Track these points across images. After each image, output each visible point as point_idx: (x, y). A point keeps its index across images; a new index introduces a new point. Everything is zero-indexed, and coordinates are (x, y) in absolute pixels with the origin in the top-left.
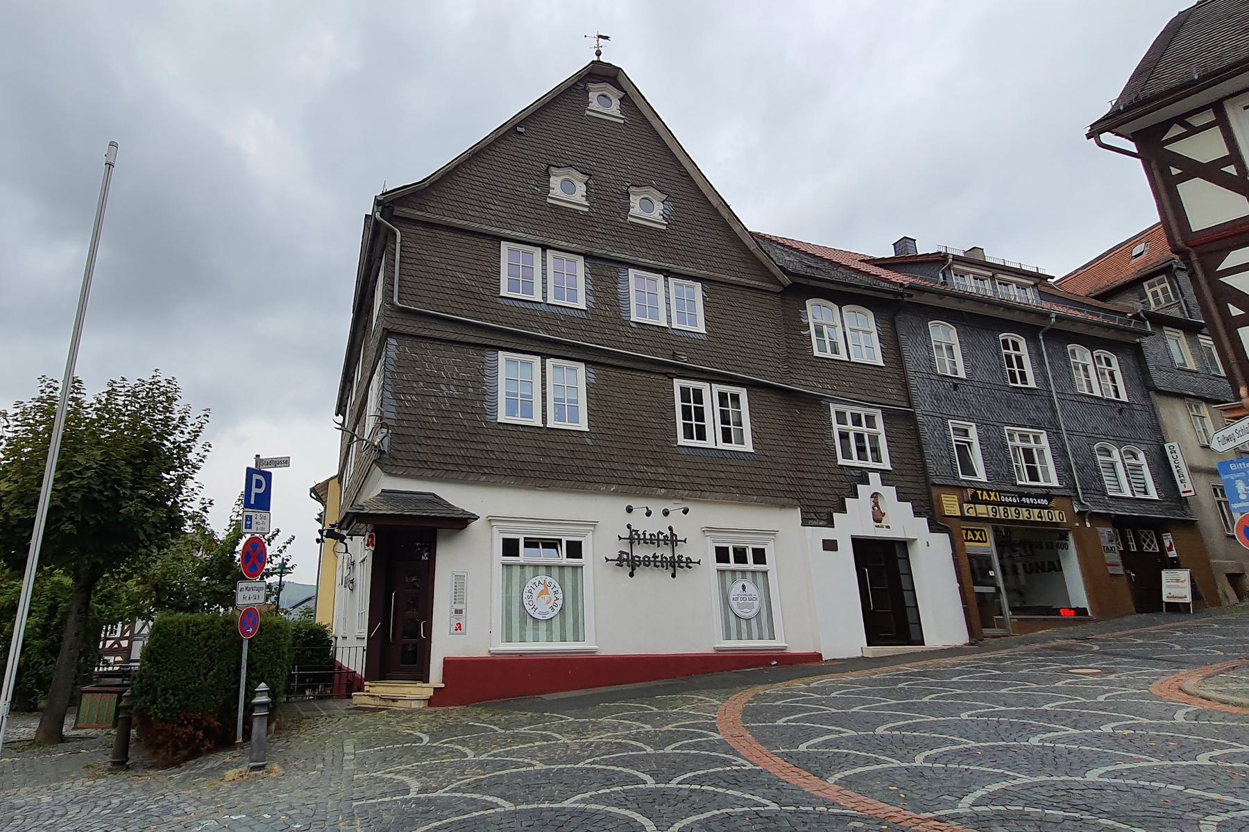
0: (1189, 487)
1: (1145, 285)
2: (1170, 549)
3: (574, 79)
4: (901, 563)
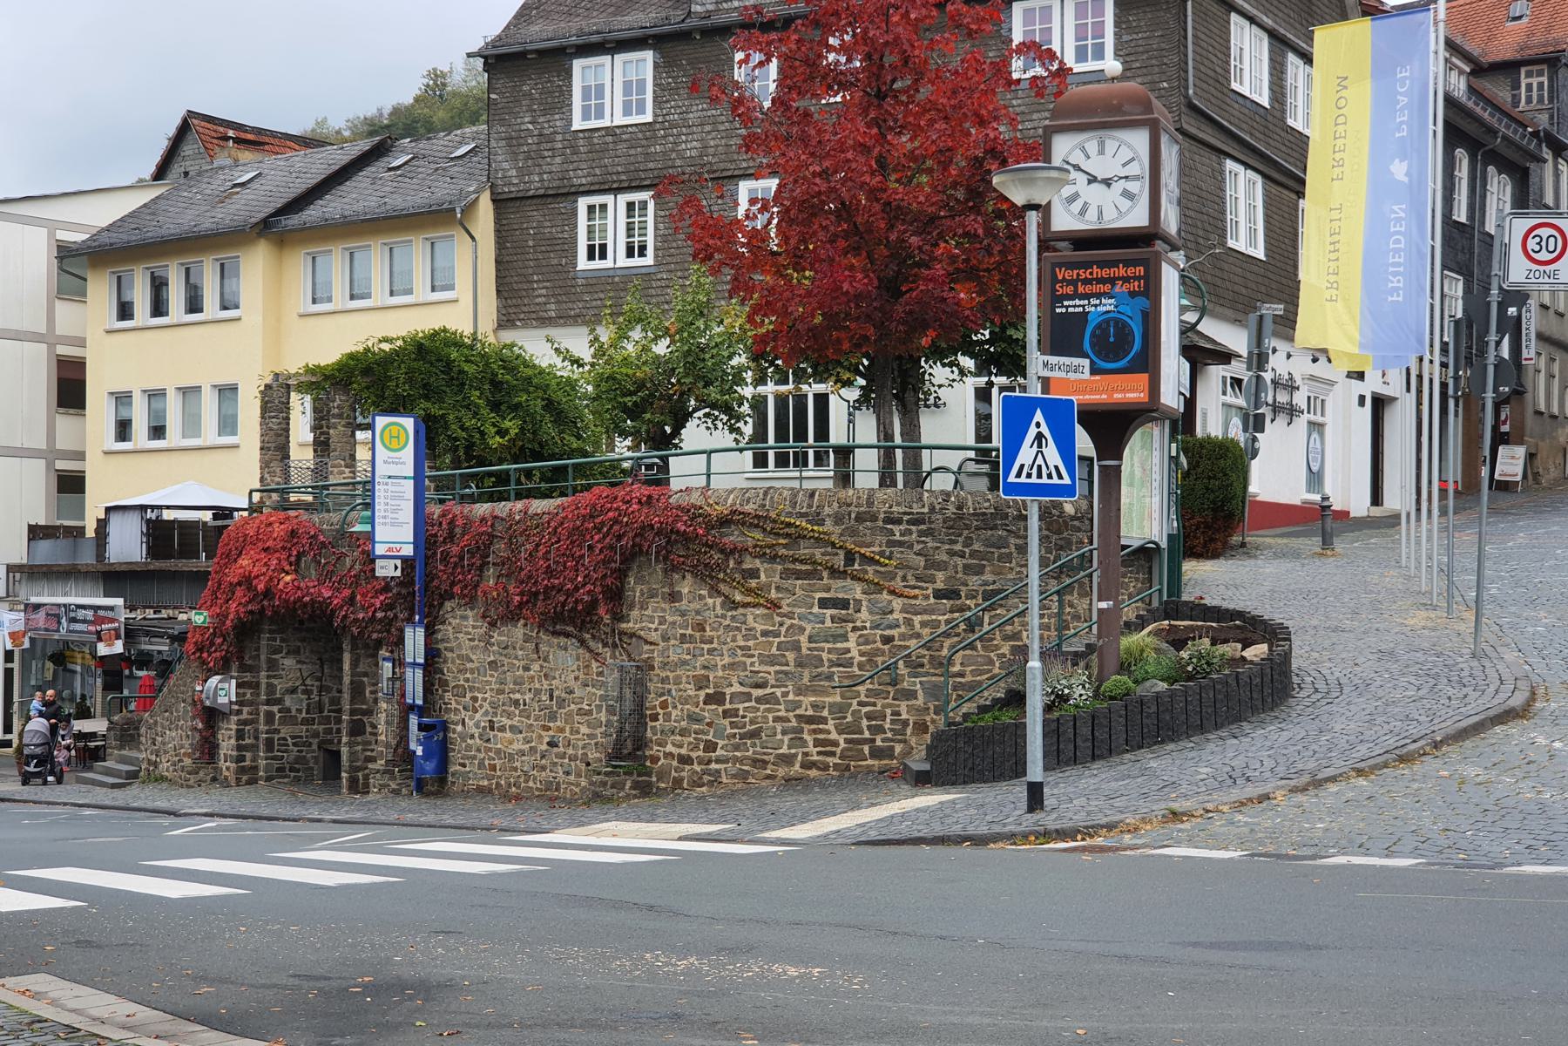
0: (1532, 355)
1: (1523, 71)
2: (1504, 423)
3: (624, 835)
4: (1229, 313)
